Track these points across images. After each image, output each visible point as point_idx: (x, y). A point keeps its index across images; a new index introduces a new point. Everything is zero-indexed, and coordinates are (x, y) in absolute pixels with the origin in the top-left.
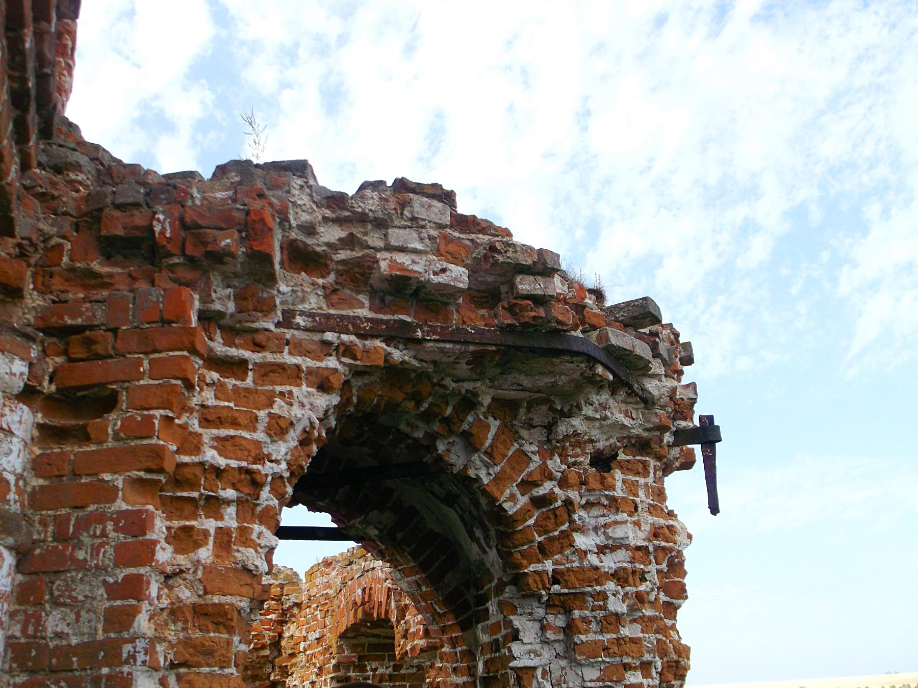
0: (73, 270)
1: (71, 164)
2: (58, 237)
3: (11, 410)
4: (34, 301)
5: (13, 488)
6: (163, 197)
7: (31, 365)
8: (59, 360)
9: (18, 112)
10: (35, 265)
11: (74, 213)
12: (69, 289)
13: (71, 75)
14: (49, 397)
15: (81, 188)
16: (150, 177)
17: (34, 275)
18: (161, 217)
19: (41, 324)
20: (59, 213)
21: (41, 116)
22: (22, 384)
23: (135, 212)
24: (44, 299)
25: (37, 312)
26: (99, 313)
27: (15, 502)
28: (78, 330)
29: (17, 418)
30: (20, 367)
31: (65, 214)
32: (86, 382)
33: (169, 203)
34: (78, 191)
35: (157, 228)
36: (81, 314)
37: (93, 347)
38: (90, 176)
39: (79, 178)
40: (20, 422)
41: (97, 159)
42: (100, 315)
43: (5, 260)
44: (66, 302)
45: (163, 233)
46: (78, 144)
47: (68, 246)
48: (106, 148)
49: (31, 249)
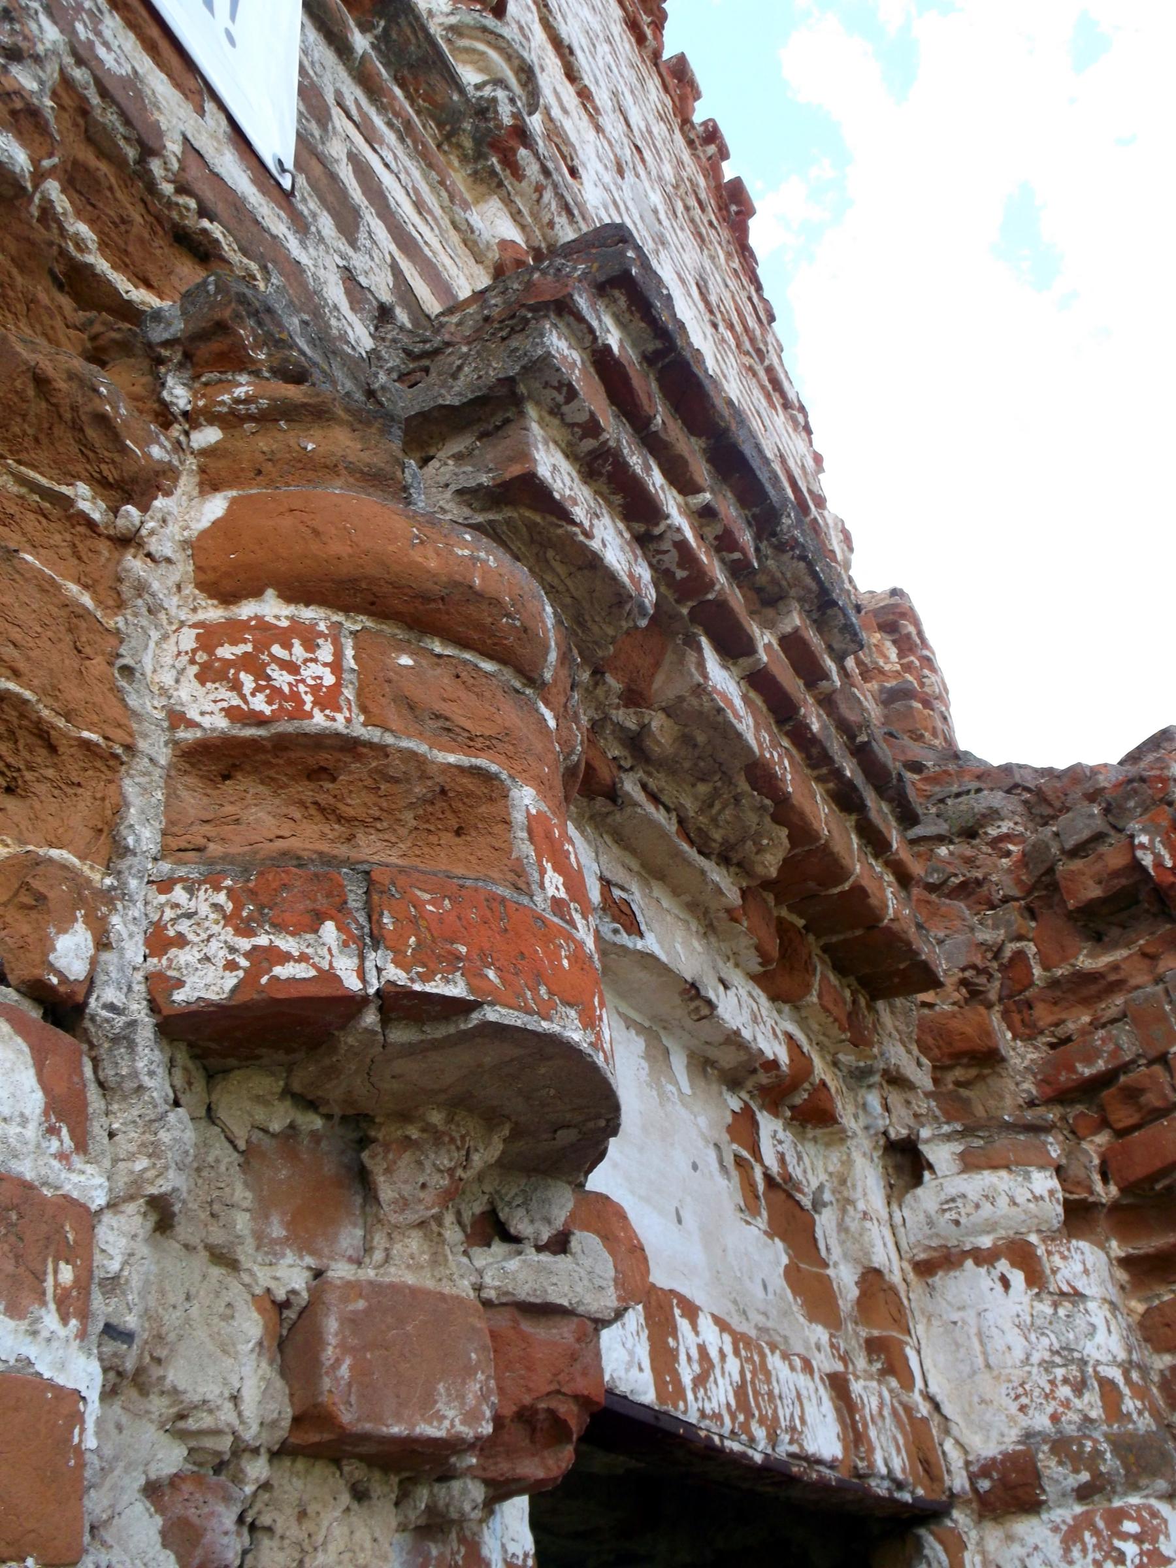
0: (1054, 983)
1: (984, 816)
2: (1011, 941)
3: (1064, 1258)
4: (1023, 1058)
5: (1126, 1390)
6: (1131, 804)
7: (1059, 1170)
8: (1102, 1138)
9: (854, 817)
10: (1000, 1000)
11: (1016, 892)
12: (1064, 1016)
13: (934, 669)
14: (1115, 1208)
15: (1011, 847)
16: (1101, 777)
17: (1006, 1015)
18: (1144, 839)
19: (1049, 1091)
20: (996, 902)
21: (890, 800)
22: (1060, 1209)
23: (1103, 849)
24: (1036, 1048)
25: (1035, 1075)
26: (1124, 1040)
27: (1140, 1413)
28: (1106, 1080)
29: (1079, 1268)
30: (1044, 1182)
31: (1006, 900)
32: (1158, 1164)
33: (1146, 810)
34: (1008, 854)
35: (1147, 860)
36: (1097, 1053)
37: (1143, 1100)
38: (1017, 819)
39: (1004, 830)
40: (1086, 1272)
41: (1016, 786)
42: (1127, 1042)
43: (954, 1015)
44: (1069, 1039)
45: (1159, 864)
46: (979, 777)
47: (1031, 949)
48: (1022, 762)
49: (982, 980)
